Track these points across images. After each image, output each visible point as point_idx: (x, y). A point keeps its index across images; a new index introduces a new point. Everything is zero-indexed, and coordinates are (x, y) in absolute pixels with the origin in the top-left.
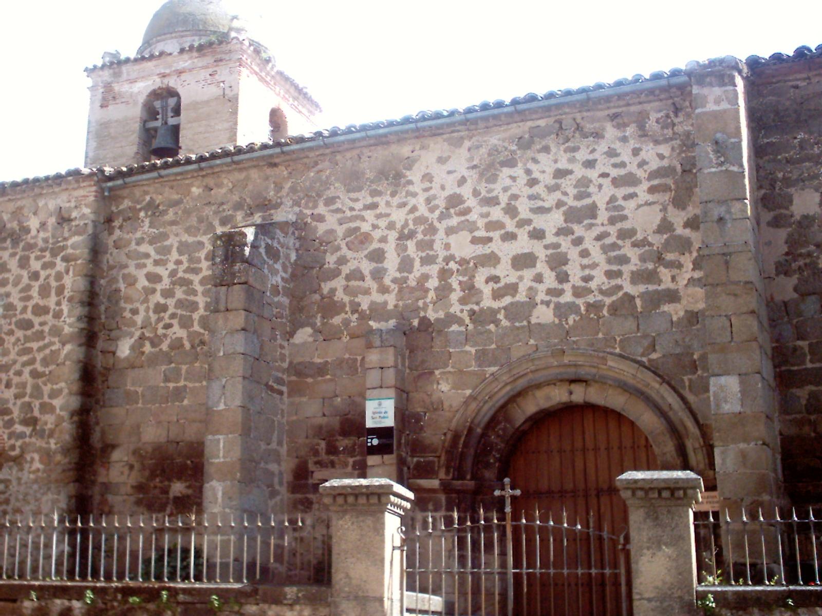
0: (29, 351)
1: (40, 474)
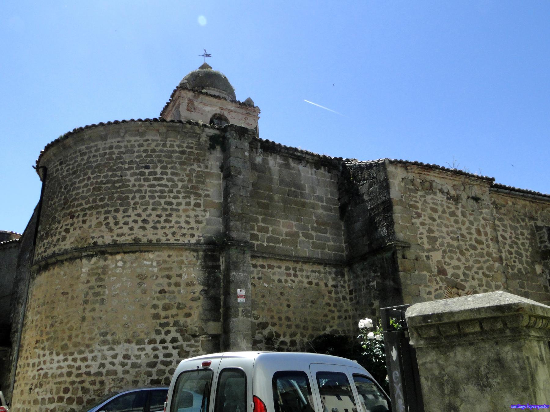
0: (478, 262)
1: (77, 180)
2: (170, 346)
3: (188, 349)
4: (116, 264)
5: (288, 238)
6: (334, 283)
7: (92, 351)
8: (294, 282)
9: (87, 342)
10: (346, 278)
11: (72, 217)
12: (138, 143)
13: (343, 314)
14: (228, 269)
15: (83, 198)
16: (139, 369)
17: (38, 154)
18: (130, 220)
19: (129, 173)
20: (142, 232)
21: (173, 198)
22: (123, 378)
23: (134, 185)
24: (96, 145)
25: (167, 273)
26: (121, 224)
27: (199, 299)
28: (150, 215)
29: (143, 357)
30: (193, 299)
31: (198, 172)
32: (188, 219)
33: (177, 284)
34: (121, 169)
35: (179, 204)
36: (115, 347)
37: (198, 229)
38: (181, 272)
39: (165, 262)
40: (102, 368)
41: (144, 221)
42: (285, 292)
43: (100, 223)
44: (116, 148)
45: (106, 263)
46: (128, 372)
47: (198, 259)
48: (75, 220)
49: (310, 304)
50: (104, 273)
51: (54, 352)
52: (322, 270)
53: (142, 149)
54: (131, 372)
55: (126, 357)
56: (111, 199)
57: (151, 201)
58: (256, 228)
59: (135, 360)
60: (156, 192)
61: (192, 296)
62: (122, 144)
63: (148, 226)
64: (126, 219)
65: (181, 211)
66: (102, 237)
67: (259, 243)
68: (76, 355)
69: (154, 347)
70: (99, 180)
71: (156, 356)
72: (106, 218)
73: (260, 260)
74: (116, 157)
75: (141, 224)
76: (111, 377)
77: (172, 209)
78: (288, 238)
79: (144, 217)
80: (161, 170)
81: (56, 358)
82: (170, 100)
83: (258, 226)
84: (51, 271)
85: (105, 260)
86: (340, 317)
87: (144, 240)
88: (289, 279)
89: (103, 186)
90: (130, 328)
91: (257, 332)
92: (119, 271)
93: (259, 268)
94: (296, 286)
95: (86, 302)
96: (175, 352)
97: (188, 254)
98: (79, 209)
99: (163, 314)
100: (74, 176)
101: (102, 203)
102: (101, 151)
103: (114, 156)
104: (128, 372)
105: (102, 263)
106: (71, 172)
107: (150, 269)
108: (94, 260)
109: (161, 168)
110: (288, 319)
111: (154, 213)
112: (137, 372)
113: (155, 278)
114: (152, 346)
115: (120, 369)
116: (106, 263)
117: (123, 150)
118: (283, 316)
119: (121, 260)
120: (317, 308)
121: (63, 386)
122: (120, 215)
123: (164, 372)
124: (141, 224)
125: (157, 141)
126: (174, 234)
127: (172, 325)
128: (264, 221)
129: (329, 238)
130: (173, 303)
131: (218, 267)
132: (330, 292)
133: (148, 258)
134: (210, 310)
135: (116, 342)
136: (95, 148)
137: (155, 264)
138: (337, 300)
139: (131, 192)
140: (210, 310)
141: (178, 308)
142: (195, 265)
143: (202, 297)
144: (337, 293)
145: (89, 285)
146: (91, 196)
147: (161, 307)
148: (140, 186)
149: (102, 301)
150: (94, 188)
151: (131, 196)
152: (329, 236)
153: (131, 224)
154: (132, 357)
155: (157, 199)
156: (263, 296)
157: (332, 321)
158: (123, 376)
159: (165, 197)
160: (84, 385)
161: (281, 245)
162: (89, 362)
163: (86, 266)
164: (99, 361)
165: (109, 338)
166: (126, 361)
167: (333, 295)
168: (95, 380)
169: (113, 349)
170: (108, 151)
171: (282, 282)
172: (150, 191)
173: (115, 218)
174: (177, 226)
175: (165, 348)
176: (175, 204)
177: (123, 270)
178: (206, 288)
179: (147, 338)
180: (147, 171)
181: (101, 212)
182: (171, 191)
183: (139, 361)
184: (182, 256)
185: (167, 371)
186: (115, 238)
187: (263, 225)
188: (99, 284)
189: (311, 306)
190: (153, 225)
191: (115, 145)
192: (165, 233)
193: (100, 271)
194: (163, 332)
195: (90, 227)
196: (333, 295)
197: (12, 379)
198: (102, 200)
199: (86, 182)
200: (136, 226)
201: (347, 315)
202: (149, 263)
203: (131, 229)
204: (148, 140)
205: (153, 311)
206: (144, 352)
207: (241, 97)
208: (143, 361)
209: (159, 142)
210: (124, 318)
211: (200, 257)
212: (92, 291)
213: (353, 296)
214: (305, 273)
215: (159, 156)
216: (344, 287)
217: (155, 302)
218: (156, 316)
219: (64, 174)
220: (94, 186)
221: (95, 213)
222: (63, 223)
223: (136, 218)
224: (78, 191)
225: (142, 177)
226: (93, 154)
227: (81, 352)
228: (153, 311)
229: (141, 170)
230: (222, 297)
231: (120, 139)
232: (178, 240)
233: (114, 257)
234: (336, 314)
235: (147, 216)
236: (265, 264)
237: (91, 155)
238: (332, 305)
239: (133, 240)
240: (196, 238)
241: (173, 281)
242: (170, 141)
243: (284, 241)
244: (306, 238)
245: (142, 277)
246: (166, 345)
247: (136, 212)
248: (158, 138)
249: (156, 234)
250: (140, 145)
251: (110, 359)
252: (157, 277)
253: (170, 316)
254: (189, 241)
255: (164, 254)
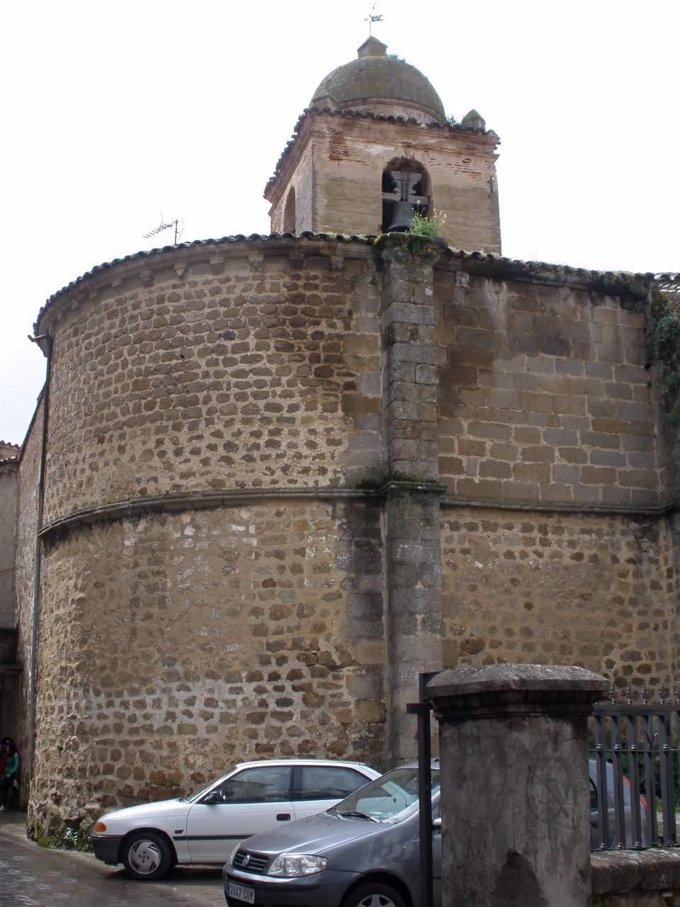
2: (288, 685)
3: (321, 691)
4: (183, 532)
5: (527, 463)
6: (631, 555)
7: (151, 692)
8: (540, 555)
9: (143, 675)
10: (662, 542)
11: (101, 441)
12: (210, 286)
13: (651, 620)
14: (392, 539)
15: (117, 402)
16: (234, 725)
17: (38, 312)
18: (202, 445)
19: (195, 349)
20: (226, 470)
21: (280, 396)
22: (207, 740)
23: (206, 375)
24: (135, 296)
25: (276, 547)
26: (186, 454)
27: (340, 596)
28: (239, 433)
29: (240, 704)
30: (329, 598)
31: (331, 336)
32: (312, 438)
33: (297, 569)
34: (181, 342)
35: (294, 408)
36: (190, 684)
37: (333, 457)
38: (302, 544)
39: (270, 525)
40: (170, 721)
41: (229, 446)
42: (520, 578)
43: (149, 453)
44: (170, 300)
45: (164, 530)
46: (215, 729)
47: (334, 517)
48: (106, 446)
49: (576, 601)
50: (163, 549)
51: (91, 690)
52: (605, 528)
53: (218, 298)
54: (219, 730)
55: (210, 702)
56: (165, 405)
57: (240, 405)
58: (456, 446)
59: (225, 710)
60: (248, 385)
61: (326, 590)
62: (179, 291)
63: (236, 456)
64: (196, 443)
65: (298, 421)
66: (155, 479)
67: (462, 477)
68: (126, 697)
69: (258, 687)
70: (143, 367)
71: (263, 704)
72: (159, 443)
73: (467, 512)
74: (171, 318)
75: (224, 453)
76: (187, 737)
77: (279, 420)
78: (527, 463)
79: (228, 437)
80: (255, 341)
81: (95, 701)
82: (293, 136)
83: (461, 442)
84: (73, 544)
85: (163, 523)
86: (643, 626)
87: (230, 485)
88: (529, 550)
89: (150, 377)
90: (215, 651)
91: (460, 659)
92: (187, 544)
93: (464, 531)
94: (546, 565)
95: (135, 602)
96: (297, 697)
97: (314, 508)
98: (111, 423)
99: (272, 625)
100: (100, 358)
101: (150, 412)
102: (144, 308)
103: (167, 317)
104: (215, 729)
105: (156, 528)
106: (93, 350)
107: (245, 540)
108: (142, 525)
109: (256, 336)
110: (527, 632)
111: (247, 429)
112: (230, 730)
113: (253, 556)
114: (254, 684)
115: (202, 725)
116: (164, 530)
117: (183, 302)
118: (516, 628)
119: (189, 524)
120: (593, 610)
121: (110, 748)
122: (183, 436)
123: (278, 731)
124: (224, 453)
125: (246, 279)
126: (285, 469)
127: (289, 644)
128: (472, 429)
129: (623, 457)
130: (289, 605)
131: (377, 533)
132: (624, 575)
133: (238, 519)
134: (363, 618)
135: (189, 676)
136: (133, 301)
137: (252, 530)
138: (640, 589)
139: (201, 387)
140: (363, 618)
141: (301, 615)
142: (329, 529)
143: (345, 594)
144: (638, 574)
145: (138, 570)
146: (130, 398)
147: (267, 612)
148: (219, 374)
149: (162, 603)
150: (135, 383)
151: (201, 395)
152: (622, 453)
153: (206, 454)
154: (221, 704)
155: (251, 399)
156: (473, 588)
157: (625, 636)
158: (207, 736)
159: (266, 396)
160: (143, 748)
161: (512, 479)
162: (149, 710)
163: (130, 536)
164: (165, 708)
165: (178, 667)
166: (209, 710)
167: (630, 579)
168: (160, 741)
169: (188, 689)
170: (155, 307)
171: (514, 557)
172: (236, 385)
173: (175, 442)
174: (291, 452)
175: (279, 689)
176: (286, 408)
177: (195, 543)
178: (353, 575)
179: (244, 670)
180: (229, 344)
181: (149, 429)
182: (277, 383)
183: (233, 711)
184: (302, 513)
185: (284, 731)
186: (178, 481)
187: (471, 437)
188: (156, 568)
189: (580, 606)
190: (244, 453)
191: (168, 293)
192: (269, 469)
193: (156, 544)
194: (273, 660)
195: (133, 459)
196: (630, 579)
197: (29, 732)
198: (150, 406)
199: (120, 370)
200: (214, 457)
201: (659, 620)
202: (242, 528)
203: (205, 462)
204: (228, 280)
205: (253, 620)
206: (241, 696)
207: (455, 112)
208: (240, 709)
209: (250, 281)
210: (202, 634)
211: (339, 513)
212: (144, 582)
213: (673, 581)
214: (566, 537)
215: (251, 311)
216: (655, 562)
217: (257, 603)
218: (259, 630)
219: (82, 354)
220: (135, 378)
221: (139, 432)
222: (87, 452)
223: (214, 440)
224: (107, 389)
225: (221, 358)
226: (128, 314)
227: (134, 692)
228: (253, 620)
229: (218, 342)
230: (385, 594)
231: (175, 281)
232: (295, 482)
233: (177, 518)
234: (636, 620)
235: (234, 435)
236: (477, 520)
237: (127, 315)
238: (627, 601)
239: (210, 484)
240: (330, 475)
241: (287, 562)
242: (271, 277)
243: (518, 470)
244: (570, 461)
245: (230, 557)
246: (279, 683)
247: (212, 429)
248: (247, 273)
249: (252, 471)
250: (215, 291)
251: (182, 707)
252: (258, 555)
253: (285, 629)
254: (316, 482)
255: (270, 510)
